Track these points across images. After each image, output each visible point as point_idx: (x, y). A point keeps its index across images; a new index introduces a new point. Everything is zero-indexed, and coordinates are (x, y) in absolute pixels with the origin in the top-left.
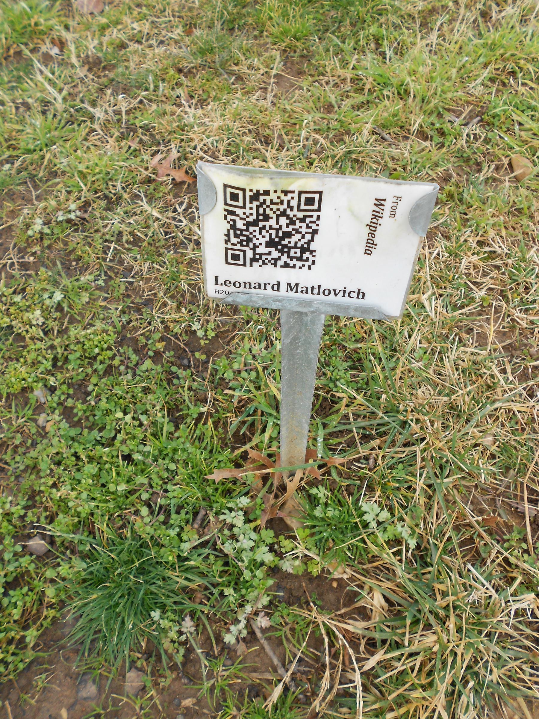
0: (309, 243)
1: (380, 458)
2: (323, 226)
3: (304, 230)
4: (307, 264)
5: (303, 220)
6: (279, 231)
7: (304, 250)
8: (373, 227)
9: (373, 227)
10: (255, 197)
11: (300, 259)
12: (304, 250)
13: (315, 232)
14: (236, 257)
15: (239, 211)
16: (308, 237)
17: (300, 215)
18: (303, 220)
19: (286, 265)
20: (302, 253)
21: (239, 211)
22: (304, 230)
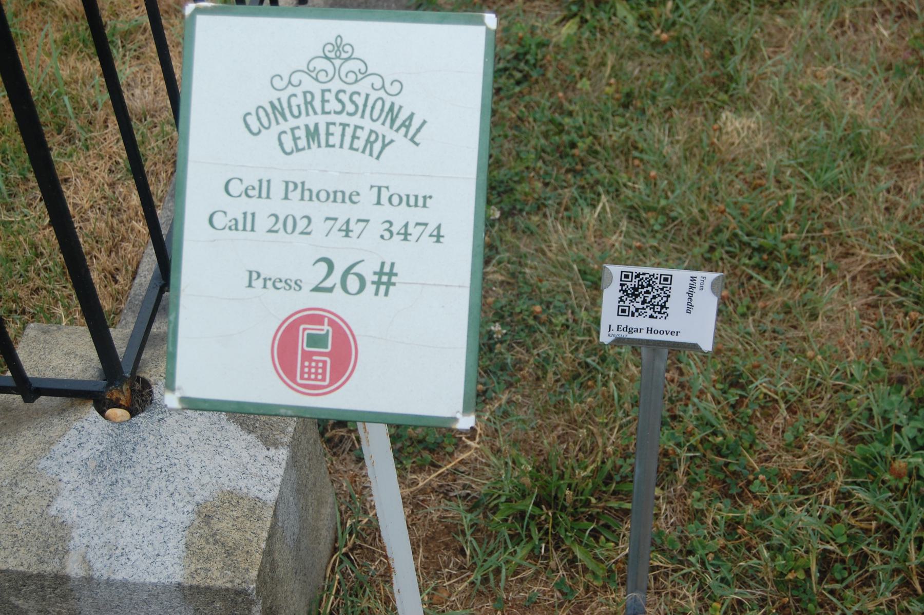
0: (665, 302)
1: (901, 299)
2: (673, 294)
3: (662, 295)
4: (664, 316)
5: (662, 289)
6: (644, 295)
7: (663, 307)
8: (690, 295)
9: (690, 295)
10: (638, 276)
11: (660, 313)
12: (663, 307)
13: (669, 296)
14: (623, 311)
15: (629, 284)
16: (665, 299)
17: (661, 286)
18: (662, 289)
19: (651, 317)
20: (662, 309)
21: (629, 284)
22: (662, 295)
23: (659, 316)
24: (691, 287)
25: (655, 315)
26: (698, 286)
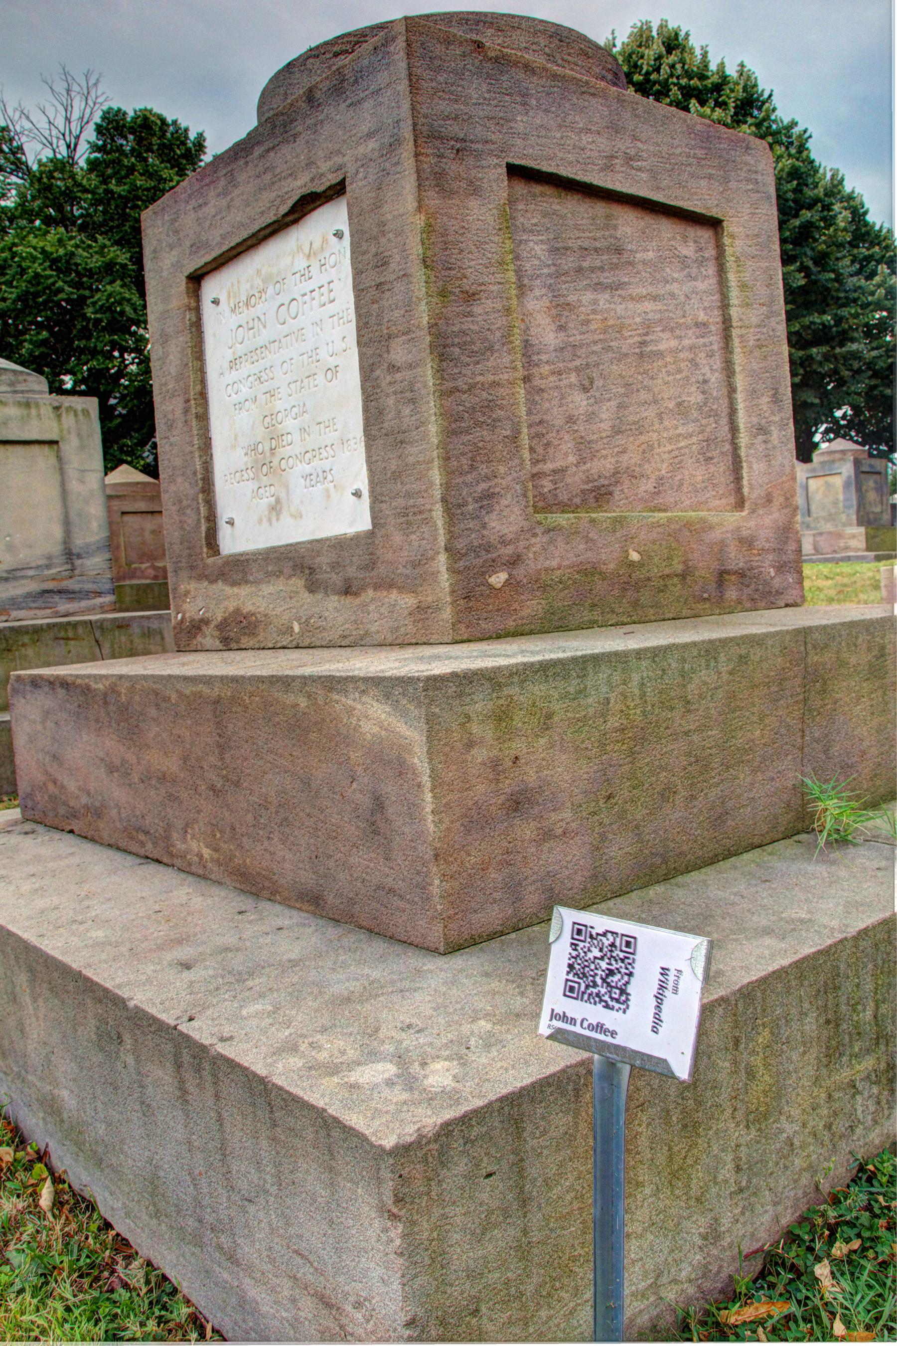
3: (623, 971)
5: (622, 960)
8: (659, 999)
9: (659, 999)
11: (617, 1001)
17: (622, 955)
20: (621, 994)
23: (617, 1006)
24: (662, 987)
25: (611, 1003)
26: (670, 986)
